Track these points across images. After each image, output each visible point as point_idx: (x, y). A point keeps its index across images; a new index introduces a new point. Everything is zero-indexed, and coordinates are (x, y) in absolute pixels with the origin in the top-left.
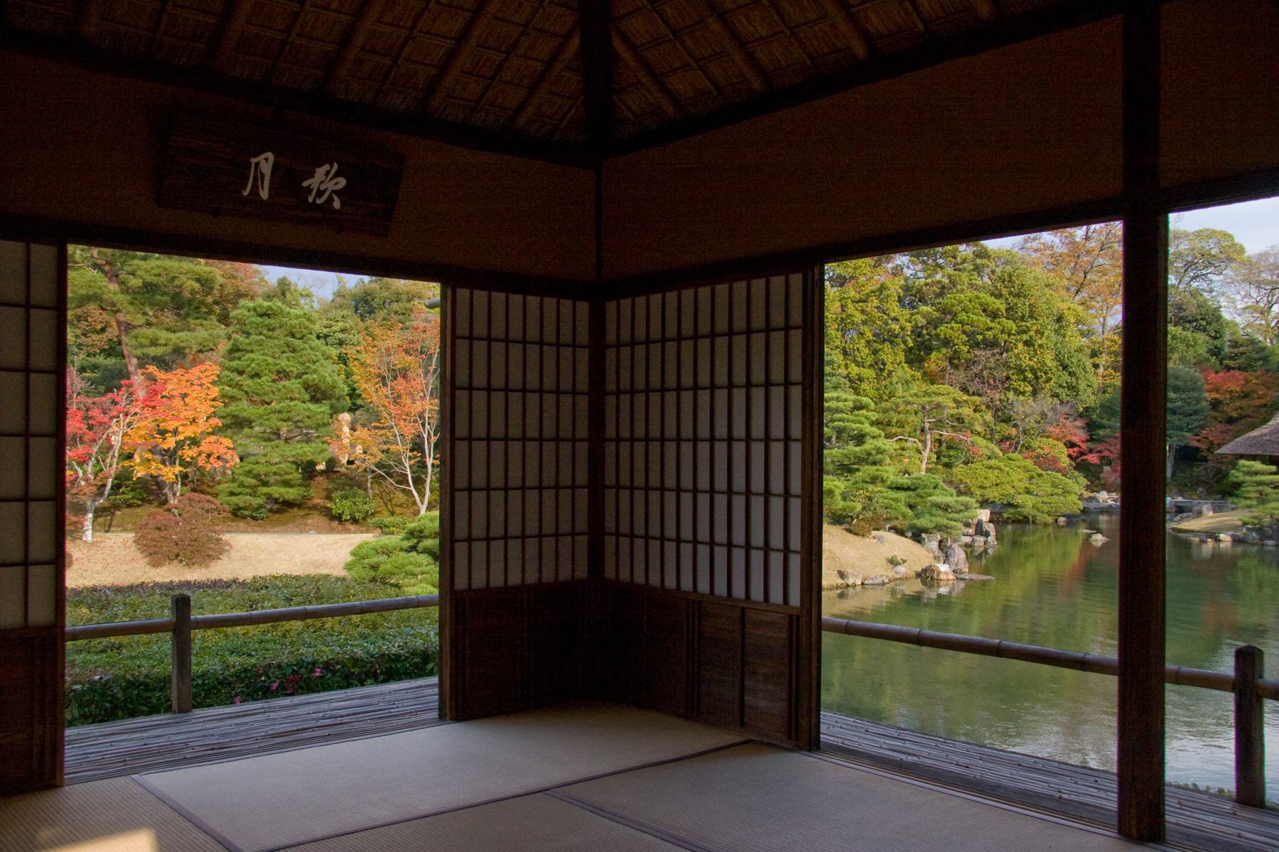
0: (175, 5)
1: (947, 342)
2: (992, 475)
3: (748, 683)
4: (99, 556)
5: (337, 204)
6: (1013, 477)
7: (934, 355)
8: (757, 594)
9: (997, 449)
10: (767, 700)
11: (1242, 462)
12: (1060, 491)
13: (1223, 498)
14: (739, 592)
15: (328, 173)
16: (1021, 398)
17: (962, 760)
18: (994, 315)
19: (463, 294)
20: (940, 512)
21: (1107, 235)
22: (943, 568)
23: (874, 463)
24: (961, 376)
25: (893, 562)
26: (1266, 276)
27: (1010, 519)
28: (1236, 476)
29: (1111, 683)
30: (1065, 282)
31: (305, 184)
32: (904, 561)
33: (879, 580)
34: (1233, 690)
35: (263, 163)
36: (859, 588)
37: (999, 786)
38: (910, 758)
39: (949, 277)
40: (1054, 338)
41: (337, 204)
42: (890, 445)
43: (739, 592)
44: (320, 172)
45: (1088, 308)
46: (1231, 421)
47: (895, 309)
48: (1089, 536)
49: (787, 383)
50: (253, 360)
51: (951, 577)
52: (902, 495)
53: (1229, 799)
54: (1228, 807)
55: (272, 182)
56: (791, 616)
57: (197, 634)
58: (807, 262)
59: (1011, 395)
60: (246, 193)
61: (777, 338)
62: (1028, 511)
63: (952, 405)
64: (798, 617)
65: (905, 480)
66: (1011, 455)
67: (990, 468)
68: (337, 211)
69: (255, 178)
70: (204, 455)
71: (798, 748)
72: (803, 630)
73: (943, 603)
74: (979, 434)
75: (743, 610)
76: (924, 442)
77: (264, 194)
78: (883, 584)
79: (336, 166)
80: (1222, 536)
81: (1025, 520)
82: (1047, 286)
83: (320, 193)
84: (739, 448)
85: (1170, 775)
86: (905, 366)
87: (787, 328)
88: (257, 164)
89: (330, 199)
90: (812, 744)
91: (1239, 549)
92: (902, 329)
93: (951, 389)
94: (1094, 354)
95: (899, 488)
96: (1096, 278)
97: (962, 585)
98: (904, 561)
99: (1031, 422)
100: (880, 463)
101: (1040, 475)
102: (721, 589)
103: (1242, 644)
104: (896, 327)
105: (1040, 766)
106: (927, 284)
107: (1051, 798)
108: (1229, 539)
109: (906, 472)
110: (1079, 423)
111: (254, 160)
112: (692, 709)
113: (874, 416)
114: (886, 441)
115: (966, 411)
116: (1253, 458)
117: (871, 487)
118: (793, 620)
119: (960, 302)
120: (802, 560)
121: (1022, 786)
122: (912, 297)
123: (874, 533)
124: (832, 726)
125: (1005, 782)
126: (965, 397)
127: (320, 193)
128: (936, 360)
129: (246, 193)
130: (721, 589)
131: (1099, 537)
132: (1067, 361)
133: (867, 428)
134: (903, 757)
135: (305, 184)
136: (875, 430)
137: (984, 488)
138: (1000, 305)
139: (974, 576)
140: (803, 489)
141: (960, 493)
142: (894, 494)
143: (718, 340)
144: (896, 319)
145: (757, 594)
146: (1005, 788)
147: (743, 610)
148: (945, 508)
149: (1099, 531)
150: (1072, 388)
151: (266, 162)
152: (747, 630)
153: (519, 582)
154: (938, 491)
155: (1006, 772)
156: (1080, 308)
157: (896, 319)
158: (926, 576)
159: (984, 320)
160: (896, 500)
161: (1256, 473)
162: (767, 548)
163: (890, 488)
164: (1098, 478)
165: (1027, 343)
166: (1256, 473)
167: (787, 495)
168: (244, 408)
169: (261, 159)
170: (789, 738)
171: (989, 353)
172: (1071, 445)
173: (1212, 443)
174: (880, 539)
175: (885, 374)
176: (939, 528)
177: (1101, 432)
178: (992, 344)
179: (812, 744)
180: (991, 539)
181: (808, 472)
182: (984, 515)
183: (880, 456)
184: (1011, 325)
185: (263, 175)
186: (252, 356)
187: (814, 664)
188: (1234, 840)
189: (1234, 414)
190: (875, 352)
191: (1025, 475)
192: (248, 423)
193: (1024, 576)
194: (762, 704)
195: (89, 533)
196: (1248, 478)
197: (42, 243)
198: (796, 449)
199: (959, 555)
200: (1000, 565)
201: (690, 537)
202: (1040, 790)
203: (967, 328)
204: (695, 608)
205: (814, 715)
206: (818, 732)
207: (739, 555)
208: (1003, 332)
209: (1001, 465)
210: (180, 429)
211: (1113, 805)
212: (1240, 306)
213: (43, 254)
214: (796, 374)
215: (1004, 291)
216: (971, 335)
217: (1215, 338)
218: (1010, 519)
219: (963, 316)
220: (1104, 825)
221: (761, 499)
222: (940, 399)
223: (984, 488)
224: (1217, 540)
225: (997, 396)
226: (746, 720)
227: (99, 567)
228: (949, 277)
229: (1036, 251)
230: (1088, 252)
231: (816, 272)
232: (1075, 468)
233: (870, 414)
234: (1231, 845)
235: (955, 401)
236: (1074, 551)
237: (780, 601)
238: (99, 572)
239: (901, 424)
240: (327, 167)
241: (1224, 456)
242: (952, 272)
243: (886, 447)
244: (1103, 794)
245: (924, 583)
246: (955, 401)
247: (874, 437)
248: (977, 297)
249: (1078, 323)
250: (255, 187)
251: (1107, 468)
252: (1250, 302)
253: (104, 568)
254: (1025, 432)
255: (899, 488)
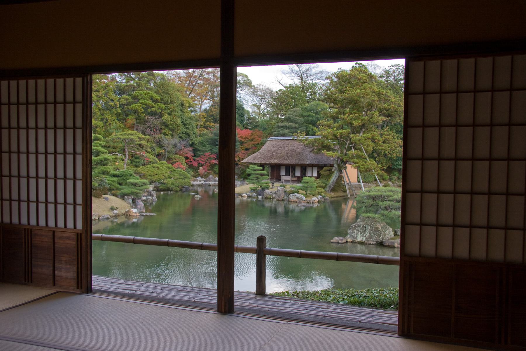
1: (135, 112)
2: (155, 170)
3: (57, 265)
6: (174, 173)
7: (130, 117)
8: (61, 224)
9: (157, 159)
10: (67, 272)
11: (251, 166)
12: (183, 177)
13: (244, 180)
14: (51, 224)
16: (166, 137)
17: (154, 291)
18: (156, 101)
20: (133, 187)
21: (213, 74)
22: (134, 210)
23: (104, 165)
24: (141, 127)
25: (112, 209)
26: (259, 93)
27: (163, 189)
28: (248, 171)
29: (215, 254)
30: (185, 89)
32: (117, 208)
33: (106, 217)
34: (256, 253)
36: (97, 221)
37: (170, 299)
38: (132, 292)
39: (137, 83)
40: (180, 113)
42: (110, 157)
43: (51, 224)
45: (194, 101)
46: (247, 149)
47: (112, 95)
48: (194, 195)
49: (75, 128)
51: (138, 214)
52: (115, 179)
53: (254, 293)
54: (254, 296)
56: (77, 233)
58: (85, 72)
59: (162, 136)
61: (70, 107)
62: (170, 185)
63: (137, 139)
64: (81, 234)
65: (117, 172)
66: (162, 162)
67: (154, 167)
71: (82, 293)
72: (84, 241)
73: (135, 225)
74: (149, 153)
75: (54, 232)
76: (125, 155)
78: (108, 218)
80: (243, 195)
81: (168, 189)
82: (178, 90)
84: (32, 157)
85: (236, 289)
86: (117, 121)
87: (75, 102)
90: (89, 290)
91: (249, 200)
92: (116, 105)
93: (138, 133)
94: (197, 120)
95: (115, 176)
96: (197, 88)
97: (143, 218)
98: (117, 208)
99: (171, 148)
100: (106, 164)
101: (175, 171)
102: (42, 223)
103: (267, 237)
104: (112, 104)
105: (185, 290)
106: (127, 86)
107: (191, 302)
108: (246, 195)
109: (118, 169)
110: (190, 149)
112: (26, 278)
113: (103, 143)
114: (109, 155)
115: (143, 142)
116: (255, 164)
117: (102, 176)
118: (79, 236)
119: (141, 94)
120: (83, 208)
121: (179, 298)
122: (121, 91)
123: (104, 196)
124: (98, 281)
125: (172, 297)
126: (143, 136)
128: (132, 119)
130: (42, 223)
131: (198, 196)
132: (185, 122)
133: (100, 149)
134: (129, 292)
136: (103, 150)
137: (151, 176)
138: (158, 97)
139: (148, 214)
140: (83, 176)
141: (142, 178)
142: (112, 179)
143: (39, 106)
144: (112, 100)
145: (61, 224)
146: (172, 300)
147: (54, 232)
148: (135, 185)
149: (198, 194)
150: (188, 135)
152: (56, 241)
154: (132, 177)
155: (172, 293)
156: (191, 101)
157: (112, 100)
158: (127, 215)
159: (150, 102)
160: (113, 181)
161: (255, 170)
162: (47, 202)
163: (111, 176)
164: (198, 172)
165: (169, 114)
166: (255, 170)
167: (75, 179)
170: (78, 288)
171: (154, 118)
172: (187, 158)
173: (240, 158)
174: (107, 199)
175: (107, 124)
176: (133, 193)
177: (199, 153)
178: (153, 114)
179: (89, 290)
180: (154, 197)
181: (85, 168)
182: (151, 188)
183: (106, 162)
184: (163, 106)
187: (89, 254)
188: (257, 308)
189: (248, 147)
190: (103, 115)
191: (168, 171)
193: (168, 213)
194: (64, 274)
196: (253, 172)
198: (79, 158)
199: (141, 204)
200: (159, 208)
201: (26, 199)
202: (186, 299)
203: (144, 106)
204: (29, 232)
205: (89, 277)
206: (91, 285)
207: (33, 206)
208: (159, 109)
209: (159, 166)
211: (216, 302)
212: (250, 104)
214: (79, 123)
215: (160, 92)
216: (146, 109)
217: (242, 116)
218: (163, 189)
219: (142, 101)
220: (212, 309)
221: (62, 181)
222: (132, 137)
223: (151, 176)
224: (242, 196)
225: (157, 136)
226: (56, 283)
228: (137, 83)
229: (173, 75)
230: (195, 77)
231: (89, 78)
232: (189, 168)
233: (102, 142)
234: (256, 310)
235: (139, 138)
236: (189, 201)
237: (63, 226)
239: (114, 148)
241: (244, 163)
242: (138, 81)
243: (109, 158)
244: (210, 298)
245: (126, 218)
246: (139, 138)
247: (103, 153)
248: (149, 93)
249: (189, 107)
251: (201, 168)
252: (254, 103)
254: (169, 152)
255: (115, 176)
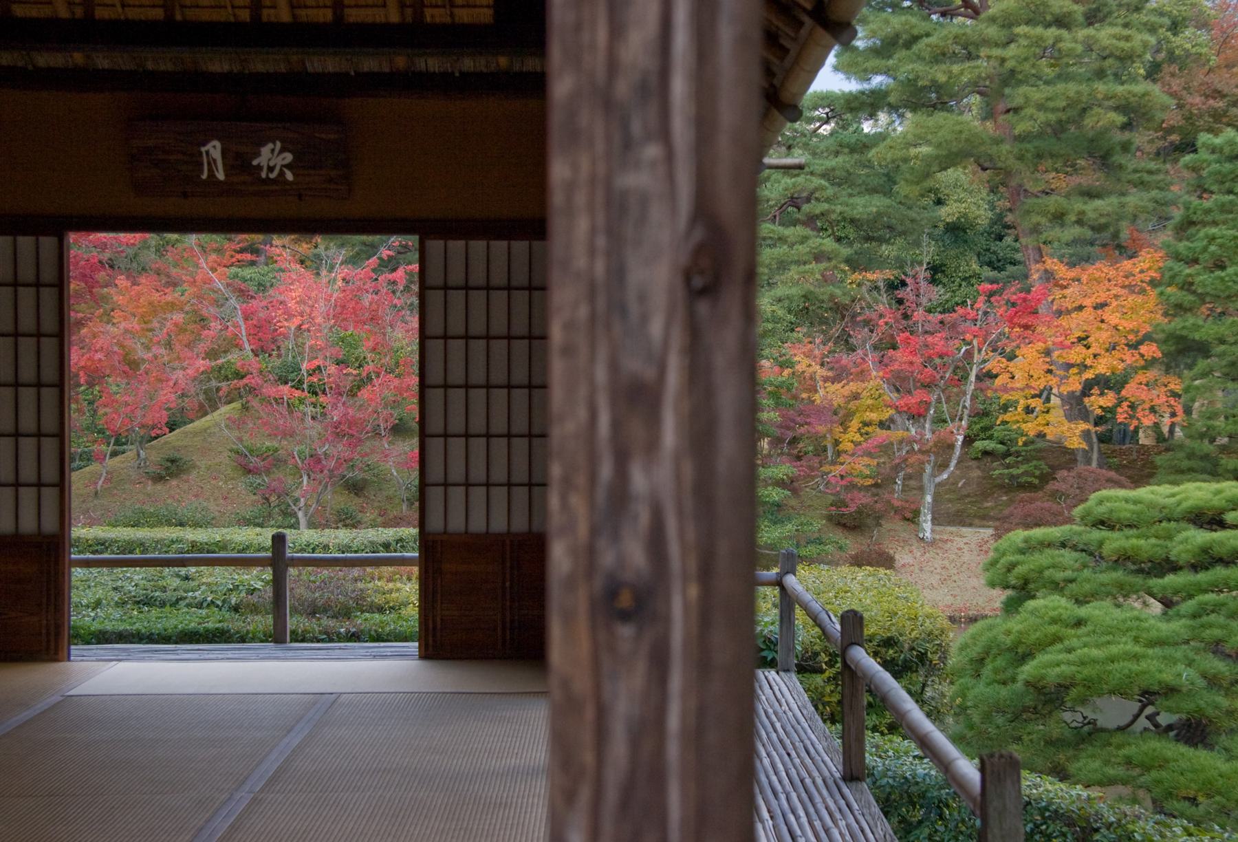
0: (182, 6)
4: (938, 563)
5: (289, 176)
15: (273, 151)
19: (436, 246)
31: (255, 163)
34: (271, 565)
35: (212, 151)
41: (289, 176)
44: (266, 151)
50: (1212, 239)
55: (224, 165)
57: (292, 571)
60: (204, 176)
68: (291, 183)
69: (209, 164)
70: (1125, 404)
77: (221, 176)
79: (278, 144)
83: (271, 169)
88: (207, 153)
89: (282, 174)
111: (203, 149)
127: (271, 169)
129: (204, 176)
135: (255, 163)
151: (214, 149)
153: (462, 529)
168: (1202, 327)
169: (209, 147)
185: (215, 161)
186: (1214, 231)
192: (1203, 349)
195: (927, 526)
197: (46, 235)
210: (635, 365)
213: (48, 243)
227: (934, 580)
238: (932, 587)
240: (270, 146)
250: (210, 170)
253: (943, 581)
